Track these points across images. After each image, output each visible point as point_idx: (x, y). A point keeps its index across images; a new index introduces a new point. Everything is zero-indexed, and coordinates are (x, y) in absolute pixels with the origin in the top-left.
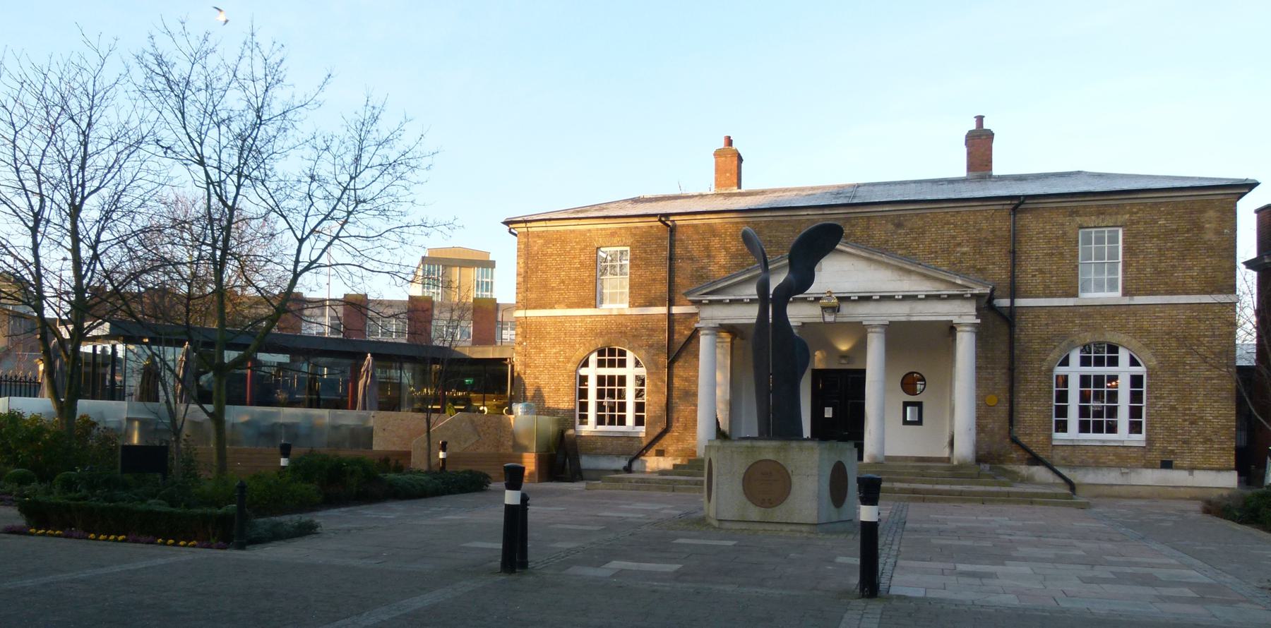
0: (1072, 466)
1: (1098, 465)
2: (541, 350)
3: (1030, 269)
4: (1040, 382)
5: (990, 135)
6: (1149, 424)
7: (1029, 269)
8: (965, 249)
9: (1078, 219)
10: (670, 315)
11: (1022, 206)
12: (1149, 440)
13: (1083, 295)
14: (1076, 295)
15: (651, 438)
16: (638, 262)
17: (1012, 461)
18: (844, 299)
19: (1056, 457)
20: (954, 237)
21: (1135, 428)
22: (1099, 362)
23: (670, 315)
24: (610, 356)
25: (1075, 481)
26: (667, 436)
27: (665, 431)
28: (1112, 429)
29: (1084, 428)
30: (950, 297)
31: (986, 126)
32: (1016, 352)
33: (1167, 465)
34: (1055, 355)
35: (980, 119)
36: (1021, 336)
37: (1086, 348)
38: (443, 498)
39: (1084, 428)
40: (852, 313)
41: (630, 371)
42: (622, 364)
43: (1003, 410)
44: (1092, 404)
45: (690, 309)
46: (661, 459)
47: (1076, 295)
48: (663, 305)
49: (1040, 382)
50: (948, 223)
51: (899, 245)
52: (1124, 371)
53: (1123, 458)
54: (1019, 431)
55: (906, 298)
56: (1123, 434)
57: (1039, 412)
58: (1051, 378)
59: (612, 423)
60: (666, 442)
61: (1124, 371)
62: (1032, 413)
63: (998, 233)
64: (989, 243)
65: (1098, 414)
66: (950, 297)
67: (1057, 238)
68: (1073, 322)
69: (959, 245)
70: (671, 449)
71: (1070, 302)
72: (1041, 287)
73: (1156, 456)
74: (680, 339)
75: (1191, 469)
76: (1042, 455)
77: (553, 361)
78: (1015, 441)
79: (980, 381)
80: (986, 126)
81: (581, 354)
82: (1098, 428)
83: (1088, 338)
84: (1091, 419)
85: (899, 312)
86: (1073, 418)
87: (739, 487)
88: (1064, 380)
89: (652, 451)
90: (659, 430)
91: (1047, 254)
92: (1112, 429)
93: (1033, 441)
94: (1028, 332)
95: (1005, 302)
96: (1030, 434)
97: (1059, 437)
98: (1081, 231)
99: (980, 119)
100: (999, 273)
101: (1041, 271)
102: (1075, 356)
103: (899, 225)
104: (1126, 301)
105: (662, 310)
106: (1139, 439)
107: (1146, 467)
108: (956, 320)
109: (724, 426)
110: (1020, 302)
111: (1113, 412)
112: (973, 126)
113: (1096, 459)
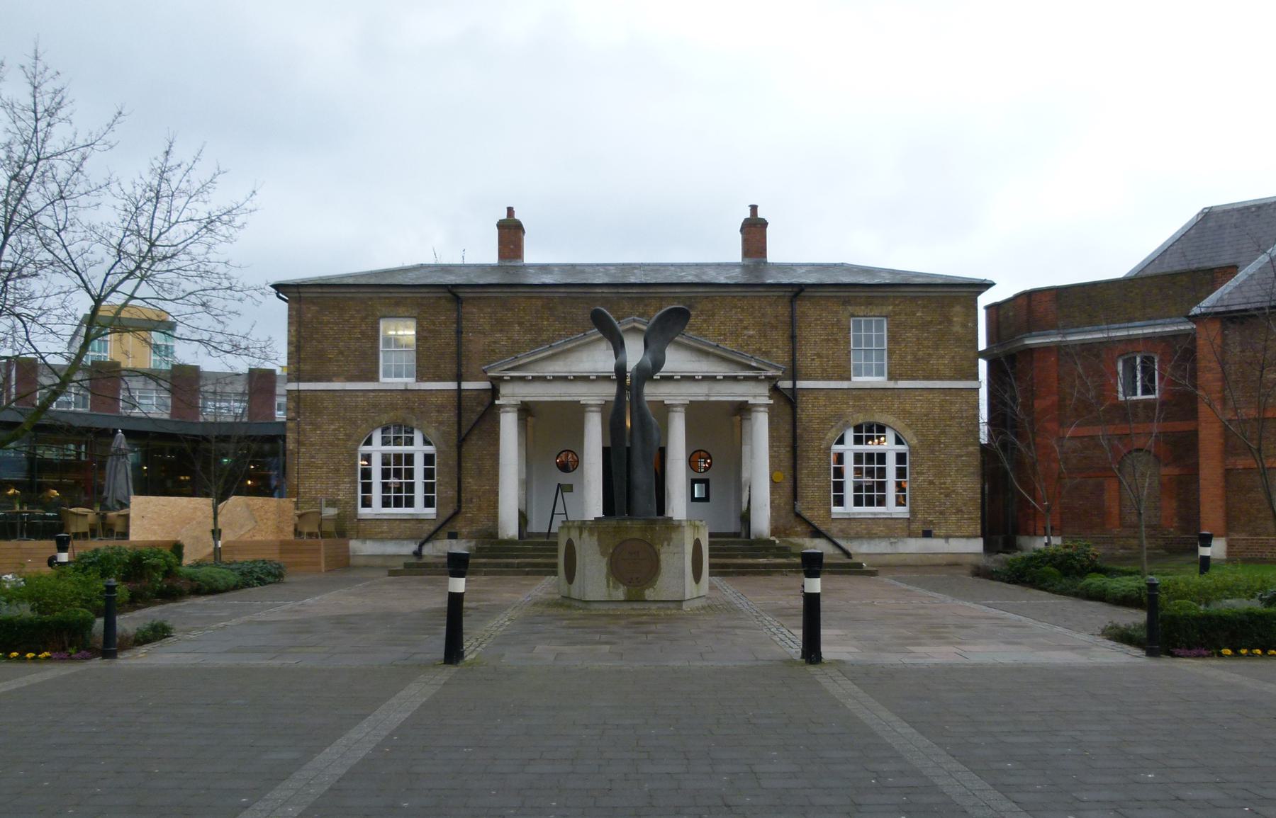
0: (849, 538)
1: (871, 536)
2: (316, 426)
3: (809, 353)
8: (751, 332)
10: (459, 390)
12: (912, 512)
15: (442, 519)
16: (425, 334)
17: (797, 535)
19: (834, 529)
20: (741, 321)
21: (429, 503)
23: (459, 390)
27: (457, 513)
29: (858, 502)
30: (746, 379)
31: (760, 215)
33: (927, 534)
34: (833, 434)
36: (802, 416)
37: (858, 428)
39: (858, 502)
41: (418, 449)
42: (410, 442)
46: (454, 541)
50: (735, 307)
52: (418, 449)
53: (890, 529)
56: (418, 508)
57: (819, 487)
60: (460, 526)
62: (812, 490)
64: (774, 327)
66: (746, 379)
69: (746, 328)
70: (465, 531)
71: (844, 385)
72: (819, 371)
73: (917, 526)
75: (947, 537)
76: (823, 528)
82: (870, 503)
83: (861, 419)
85: (699, 392)
88: (840, 458)
89: (444, 533)
94: (809, 413)
95: (786, 384)
97: (363, 512)
102: (850, 435)
104: (891, 385)
105: (452, 385)
106: (903, 512)
107: (910, 536)
108: (751, 401)
110: (802, 384)
111: (411, 488)
112: (504, 216)
113: (868, 529)
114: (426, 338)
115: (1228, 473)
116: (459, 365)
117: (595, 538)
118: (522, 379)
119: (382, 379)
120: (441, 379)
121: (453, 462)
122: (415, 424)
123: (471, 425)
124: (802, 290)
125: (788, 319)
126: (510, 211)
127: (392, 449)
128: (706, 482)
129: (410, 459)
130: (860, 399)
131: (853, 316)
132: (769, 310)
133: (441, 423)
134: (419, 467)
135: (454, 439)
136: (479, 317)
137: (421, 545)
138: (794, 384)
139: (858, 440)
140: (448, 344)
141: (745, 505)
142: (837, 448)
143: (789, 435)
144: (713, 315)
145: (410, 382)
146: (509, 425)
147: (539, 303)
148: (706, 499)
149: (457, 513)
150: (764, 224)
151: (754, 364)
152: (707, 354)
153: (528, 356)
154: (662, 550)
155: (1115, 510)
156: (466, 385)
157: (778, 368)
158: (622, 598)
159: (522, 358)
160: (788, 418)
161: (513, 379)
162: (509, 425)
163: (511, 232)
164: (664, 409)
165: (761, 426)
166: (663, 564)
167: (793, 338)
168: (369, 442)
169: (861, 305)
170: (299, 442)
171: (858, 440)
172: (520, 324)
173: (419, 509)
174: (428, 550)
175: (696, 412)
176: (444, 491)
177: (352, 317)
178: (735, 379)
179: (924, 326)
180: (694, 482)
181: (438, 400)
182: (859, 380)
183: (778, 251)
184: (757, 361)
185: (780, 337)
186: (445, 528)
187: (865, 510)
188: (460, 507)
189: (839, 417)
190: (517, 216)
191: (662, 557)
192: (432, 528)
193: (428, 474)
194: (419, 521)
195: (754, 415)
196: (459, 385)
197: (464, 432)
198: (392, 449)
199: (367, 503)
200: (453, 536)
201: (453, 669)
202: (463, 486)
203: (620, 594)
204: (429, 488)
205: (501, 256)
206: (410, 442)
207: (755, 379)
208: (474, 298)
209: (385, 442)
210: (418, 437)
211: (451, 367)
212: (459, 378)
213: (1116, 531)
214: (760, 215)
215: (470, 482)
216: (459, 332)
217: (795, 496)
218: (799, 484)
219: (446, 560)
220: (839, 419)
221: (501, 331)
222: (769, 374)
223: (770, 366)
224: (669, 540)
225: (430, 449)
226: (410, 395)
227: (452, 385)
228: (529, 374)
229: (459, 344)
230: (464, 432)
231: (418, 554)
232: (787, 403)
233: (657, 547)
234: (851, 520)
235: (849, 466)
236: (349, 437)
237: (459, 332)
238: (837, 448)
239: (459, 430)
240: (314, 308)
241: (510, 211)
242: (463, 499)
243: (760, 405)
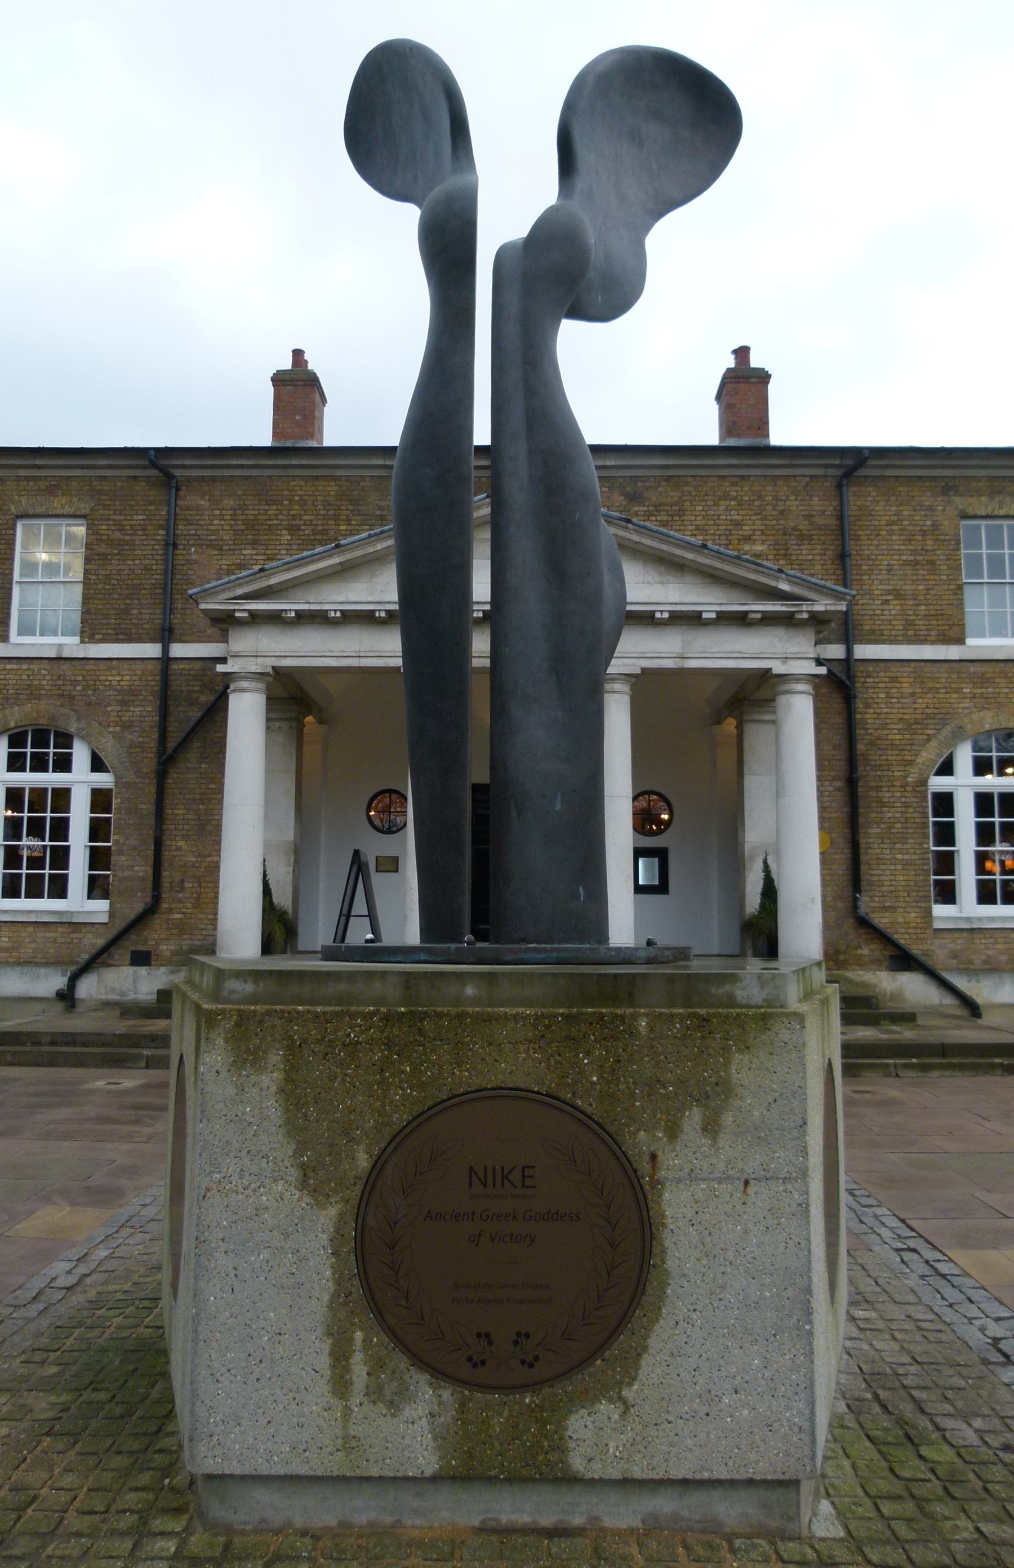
0: (970, 971)
3: (878, 589)
4: (906, 805)
8: (759, 548)
9: (957, 500)
10: (166, 660)
11: (861, 472)
13: (970, 641)
14: (960, 641)
15: (120, 924)
16: (103, 549)
17: (861, 963)
19: (939, 954)
20: (738, 524)
21: (96, 888)
22: (39, 765)
23: (166, 660)
24: (39, 745)
25: (979, 1001)
26: (157, 921)
27: (151, 911)
28: (59, 889)
29: (986, 895)
32: (860, 747)
34: (930, 754)
36: (867, 716)
39: (986, 895)
42: (64, 764)
44: (25, 842)
46: (142, 971)
47: (960, 641)
48: (153, 640)
49: (906, 805)
50: (725, 497)
52: (81, 780)
57: (906, 864)
58: (925, 798)
60: (156, 936)
62: (894, 866)
63: (818, 520)
64: (803, 538)
65: (35, 862)
66: (769, 620)
67: (924, 533)
68: (958, 691)
69: (747, 539)
70: (166, 949)
71: (952, 652)
72: (899, 625)
74: (188, 714)
76: (916, 950)
78: (863, 923)
82: (35, 891)
84: (24, 871)
86: (966, 877)
88: (944, 803)
89: (123, 953)
90: (139, 907)
91: (906, 563)
92: (59, 889)
93: (897, 921)
94: (879, 709)
96: (892, 909)
97: (940, 911)
98: (964, 522)
101: (898, 594)
102: (964, 757)
105: (152, 650)
108: (778, 668)
109: (283, 898)
110: (864, 651)
111: (61, 857)
112: (287, 364)
114: (104, 557)
116: (168, 610)
117: (270, 1080)
118: (275, 619)
119: (14, 637)
120: (129, 638)
121: (147, 807)
122: (73, 728)
123: (184, 729)
125: (834, 522)
128: (661, 855)
129: (62, 797)
131: (965, 516)
132: (793, 503)
133: (127, 726)
134: (80, 816)
135: (149, 762)
136: (208, 511)
138: (849, 651)
139: (981, 767)
140: (147, 568)
141: (753, 901)
142: (939, 783)
144: (681, 513)
145: (71, 645)
146: (246, 716)
147: (333, 488)
148: (662, 888)
149: (151, 911)
150: (763, 377)
151: (784, 586)
153: (289, 566)
154: (673, 1161)
156: (179, 650)
158: (425, 1460)
159: (276, 570)
161: (256, 619)
162: (246, 716)
165: (799, 715)
166: (680, 1249)
169: (979, 493)
171: (981, 767)
172: (293, 530)
173: (78, 902)
174: (88, 988)
176: (131, 866)
178: (741, 620)
180: (639, 853)
182: (980, 644)
184: (792, 580)
186: (123, 943)
188: (157, 899)
190: (313, 365)
191: (675, 1205)
192: (101, 942)
193: (98, 830)
194: (74, 926)
195: (782, 700)
196: (165, 651)
197: (171, 745)
200: (141, 959)
202: (166, 855)
203: (414, 1428)
204: (98, 858)
206: (64, 764)
207: (787, 621)
208: (202, 479)
210: (80, 755)
211: (151, 615)
212: (167, 635)
214: (756, 361)
215: (180, 848)
216: (171, 544)
217: (856, 881)
218: (863, 858)
219: (155, 997)
220: (944, 722)
221: (254, 543)
222: (819, 608)
223: (820, 589)
224: (714, 1096)
225: (104, 780)
226: (65, 666)
227: (152, 650)
228: (289, 606)
229: (170, 570)
230: (171, 745)
231: (67, 997)
232: (839, 687)
233: (642, 1141)
234: (973, 931)
235: (965, 820)
237: (171, 544)
238: (939, 783)
241: (298, 355)
242: (166, 884)
243: (796, 678)
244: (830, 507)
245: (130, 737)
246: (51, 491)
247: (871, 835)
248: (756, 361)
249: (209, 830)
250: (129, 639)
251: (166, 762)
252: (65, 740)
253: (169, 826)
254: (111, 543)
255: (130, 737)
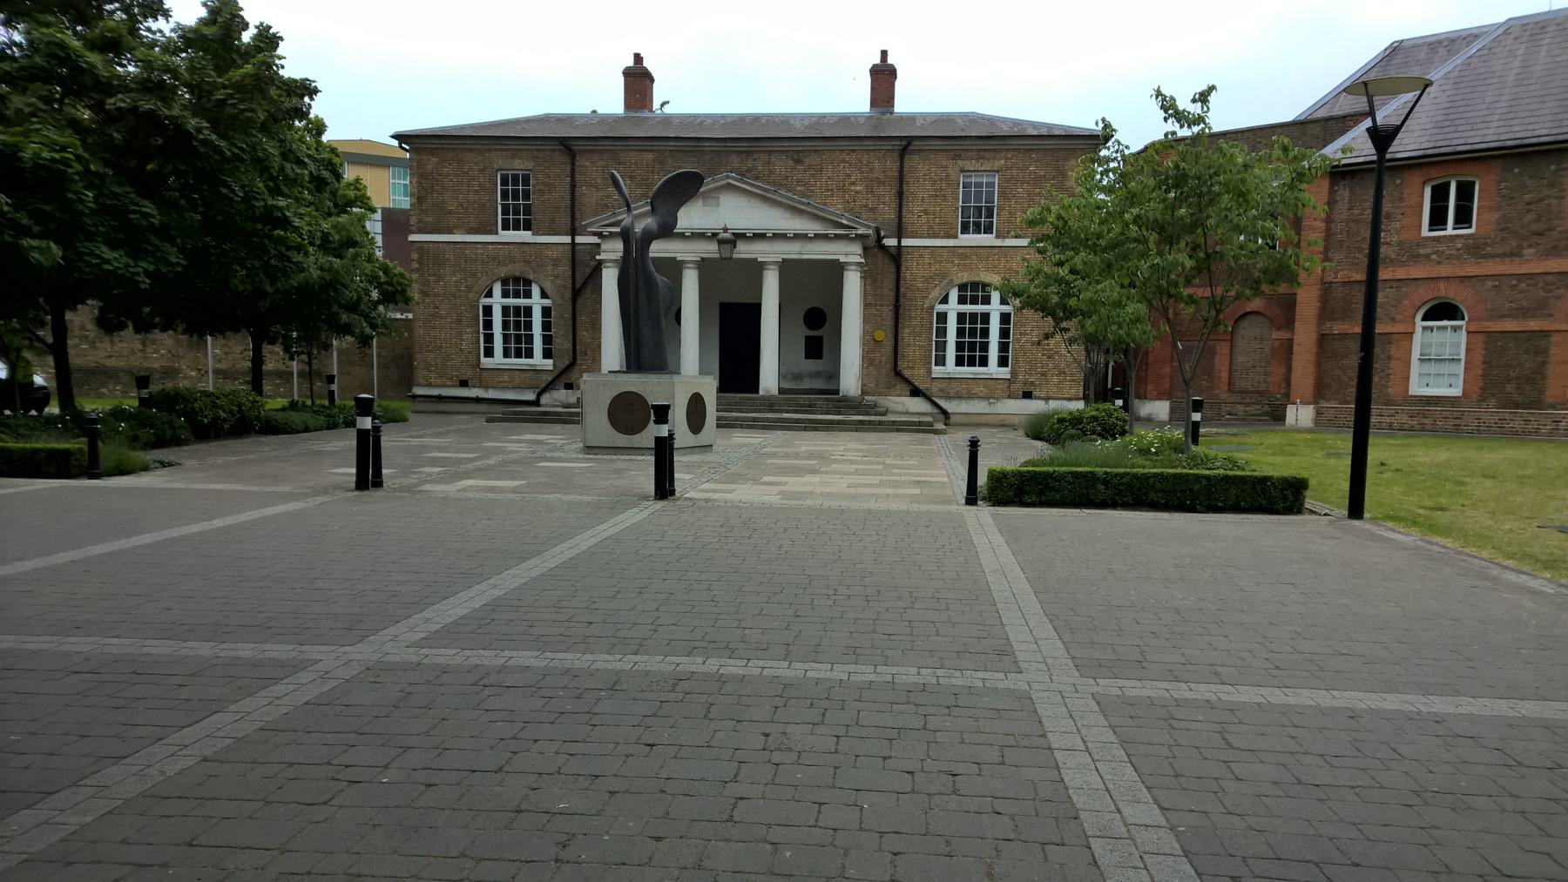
0: (948, 398)
1: (970, 396)
2: (439, 278)
3: (916, 209)
5: (892, 72)
6: (1015, 359)
7: (914, 210)
10: (573, 244)
12: (1013, 373)
18: (740, 236)
19: (934, 389)
21: (547, 354)
22: (974, 301)
23: (573, 244)
30: (837, 237)
31: (890, 61)
33: (1027, 395)
34: (936, 293)
35: (884, 54)
36: (907, 274)
37: (962, 287)
38: (265, 439)
39: (506, 354)
40: (744, 250)
41: (536, 302)
43: (889, 344)
45: (595, 240)
51: (799, 181)
52: (536, 302)
53: (991, 389)
54: (902, 364)
55: (797, 237)
56: (993, 369)
59: (518, 355)
61: (995, 308)
62: (912, 347)
64: (881, 183)
65: (972, 347)
66: (837, 237)
71: (951, 242)
73: (1018, 387)
74: (583, 272)
75: (1047, 399)
76: (921, 387)
77: (454, 289)
79: (866, 319)
80: (890, 61)
81: (484, 282)
82: (972, 363)
83: (965, 277)
85: (793, 251)
87: (605, 417)
92: (984, 362)
93: (916, 375)
94: (913, 271)
95: (891, 242)
97: (937, 371)
99: (884, 54)
100: (888, 213)
101: (926, 212)
102: (954, 295)
103: (798, 161)
104: (999, 243)
105: (567, 239)
106: (1004, 372)
107: (1009, 397)
108: (842, 259)
110: (906, 242)
112: (631, 63)
113: (965, 390)
115: (1323, 339)
121: (568, 315)
124: (909, 144)
126: (638, 58)
127: (968, 308)
129: (986, 317)
130: (966, 257)
133: (557, 277)
135: (568, 294)
136: (591, 168)
137: (539, 395)
139: (962, 300)
142: (940, 308)
143: (892, 294)
147: (650, 156)
152: (800, 212)
155: (1225, 376)
156: (579, 239)
157: (868, 227)
160: (893, 276)
163: (638, 80)
164: (674, 268)
167: (900, 194)
168: (489, 294)
170: (424, 294)
171: (962, 300)
175: (788, 269)
176: (562, 343)
177: (471, 169)
178: (825, 237)
179: (1037, 180)
181: (554, 253)
183: (907, 100)
185: (888, 194)
187: (966, 371)
188: (575, 359)
189: (943, 276)
193: (546, 326)
197: (578, 286)
198: (968, 308)
199: (489, 352)
201: (660, 504)
204: (547, 340)
205: (628, 106)
206: (528, 295)
209: (505, 295)
210: (536, 291)
212: (573, 232)
213: (1224, 396)
215: (583, 334)
216: (573, 187)
225: (547, 302)
227: (567, 239)
230: (578, 286)
232: (886, 261)
236: (470, 288)
237: (573, 187)
239: (574, 283)
240: (435, 160)
241: (638, 58)
244: (896, 167)
245: (559, 282)
246: (513, 157)
247: (905, 333)
248: (1166, 91)
249: (596, 326)
250: (555, 234)
251: (576, 293)
252: (528, 283)
253: (578, 325)
254: (544, 184)
255: (559, 282)
